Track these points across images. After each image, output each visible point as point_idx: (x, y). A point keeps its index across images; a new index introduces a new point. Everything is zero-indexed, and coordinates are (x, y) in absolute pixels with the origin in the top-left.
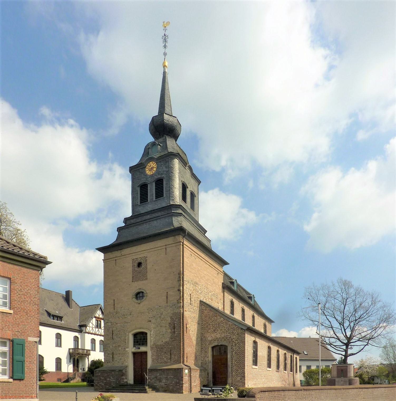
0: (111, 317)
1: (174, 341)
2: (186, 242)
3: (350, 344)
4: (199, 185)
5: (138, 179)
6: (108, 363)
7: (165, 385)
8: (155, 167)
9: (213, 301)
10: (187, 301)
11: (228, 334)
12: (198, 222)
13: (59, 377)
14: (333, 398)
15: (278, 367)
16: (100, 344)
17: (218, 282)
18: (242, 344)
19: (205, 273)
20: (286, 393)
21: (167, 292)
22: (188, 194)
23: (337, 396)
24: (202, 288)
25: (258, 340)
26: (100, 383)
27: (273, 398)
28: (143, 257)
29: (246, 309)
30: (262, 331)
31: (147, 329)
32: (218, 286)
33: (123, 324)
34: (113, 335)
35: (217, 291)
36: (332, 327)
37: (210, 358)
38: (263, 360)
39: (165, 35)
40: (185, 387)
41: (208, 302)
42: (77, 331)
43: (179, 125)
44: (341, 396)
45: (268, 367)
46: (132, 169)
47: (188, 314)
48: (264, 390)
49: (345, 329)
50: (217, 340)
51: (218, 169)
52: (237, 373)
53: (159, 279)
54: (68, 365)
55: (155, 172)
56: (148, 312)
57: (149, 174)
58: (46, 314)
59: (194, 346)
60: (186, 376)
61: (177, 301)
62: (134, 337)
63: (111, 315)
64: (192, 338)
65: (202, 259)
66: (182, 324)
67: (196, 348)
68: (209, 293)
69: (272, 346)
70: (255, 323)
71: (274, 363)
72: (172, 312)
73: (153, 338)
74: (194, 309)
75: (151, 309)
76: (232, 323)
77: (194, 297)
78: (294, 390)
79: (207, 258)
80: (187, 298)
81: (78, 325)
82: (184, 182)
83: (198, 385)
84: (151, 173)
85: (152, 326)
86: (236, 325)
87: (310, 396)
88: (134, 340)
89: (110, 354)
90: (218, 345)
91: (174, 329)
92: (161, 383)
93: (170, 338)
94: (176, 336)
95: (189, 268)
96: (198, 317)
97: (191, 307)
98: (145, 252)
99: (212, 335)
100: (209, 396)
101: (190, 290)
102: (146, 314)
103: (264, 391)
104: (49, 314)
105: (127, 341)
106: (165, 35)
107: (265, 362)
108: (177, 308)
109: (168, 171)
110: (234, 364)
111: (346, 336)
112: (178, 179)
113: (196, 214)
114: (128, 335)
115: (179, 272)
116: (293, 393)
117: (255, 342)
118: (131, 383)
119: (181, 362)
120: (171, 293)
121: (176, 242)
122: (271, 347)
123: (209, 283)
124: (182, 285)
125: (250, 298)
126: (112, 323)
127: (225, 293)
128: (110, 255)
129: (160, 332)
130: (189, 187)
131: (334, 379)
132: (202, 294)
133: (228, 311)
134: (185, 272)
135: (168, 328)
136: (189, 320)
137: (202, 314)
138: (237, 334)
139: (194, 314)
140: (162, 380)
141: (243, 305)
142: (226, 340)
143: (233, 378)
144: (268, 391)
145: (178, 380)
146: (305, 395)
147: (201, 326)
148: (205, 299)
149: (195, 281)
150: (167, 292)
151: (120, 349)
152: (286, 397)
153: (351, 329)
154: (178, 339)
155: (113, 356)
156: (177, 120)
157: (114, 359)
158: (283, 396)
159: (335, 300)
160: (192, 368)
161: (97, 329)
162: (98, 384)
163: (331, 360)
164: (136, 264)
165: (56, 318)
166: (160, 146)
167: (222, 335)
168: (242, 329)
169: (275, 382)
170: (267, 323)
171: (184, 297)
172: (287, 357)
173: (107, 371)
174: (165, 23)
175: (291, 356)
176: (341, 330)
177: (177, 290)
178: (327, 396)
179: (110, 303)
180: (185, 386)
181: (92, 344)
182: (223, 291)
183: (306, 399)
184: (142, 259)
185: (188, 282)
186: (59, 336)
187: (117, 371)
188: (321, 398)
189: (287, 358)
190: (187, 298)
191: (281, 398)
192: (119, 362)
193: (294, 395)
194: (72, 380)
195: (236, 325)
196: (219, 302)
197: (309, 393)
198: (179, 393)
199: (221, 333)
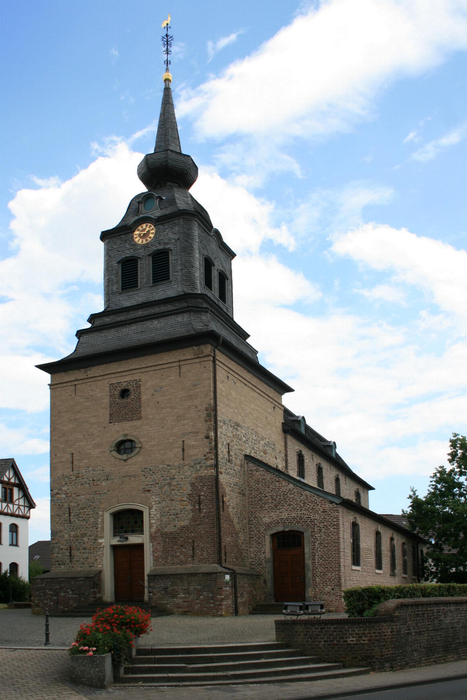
5: (118, 251)
6: (59, 564)
7: (184, 602)
9: (267, 454)
11: (305, 512)
12: (232, 319)
16: (10, 531)
18: (333, 528)
19: (253, 406)
21: (183, 441)
22: (215, 275)
24: (248, 433)
26: (46, 601)
28: (132, 381)
32: (274, 429)
34: (70, 515)
38: (369, 555)
40: (225, 605)
41: (258, 457)
47: (226, 479)
52: (324, 578)
53: (167, 419)
55: (152, 240)
57: (140, 242)
60: (227, 586)
61: (205, 456)
64: (234, 519)
65: (247, 383)
68: (260, 441)
71: (386, 561)
73: (154, 519)
74: (235, 470)
75: (150, 470)
77: (235, 449)
82: (208, 256)
84: (144, 241)
85: (153, 499)
89: (65, 549)
90: (285, 530)
91: (200, 503)
92: (175, 600)
93: (191, 519)
95: (225, 399)
98: (136, 371)
99: (272, 514)
101: (228, 437)
102: (140, 478)
105: (99, 526)
107: (372, 559)
108: (204, 467)
113: (229, 307)
114: (103, 516)
117: (355, 526)
120: (191, 442)
122: (381, 533)
123: (260, 425)
126: (68, 495)
129: (169, 510)
130: (216, 264)
132: (248, 444)
133: (293, 473)
134: (219, 405)
135: (186, 503)
136: (228, 490)
137: (250, 477)
138: (321, 512)
139: (236, 478)
140: (177, 593)
142: (300, 522)
143: (317, 589)
145: (212, 593)
148: (253, 451)
149: (235, 420)
150: (183, 441)
151: (87, 540)
154: (208, 522)
155: (70, 553)
157: (73, 558)
161: (4, 505)
162: (41, 603)
164: (117, 393)
173: (61, 579)
177: (203, 437)
179: (64, 459)
180: (226, 603)
184: (131, 384)
185: (224, 424)
196: (277, 457)
199: (290, 510)
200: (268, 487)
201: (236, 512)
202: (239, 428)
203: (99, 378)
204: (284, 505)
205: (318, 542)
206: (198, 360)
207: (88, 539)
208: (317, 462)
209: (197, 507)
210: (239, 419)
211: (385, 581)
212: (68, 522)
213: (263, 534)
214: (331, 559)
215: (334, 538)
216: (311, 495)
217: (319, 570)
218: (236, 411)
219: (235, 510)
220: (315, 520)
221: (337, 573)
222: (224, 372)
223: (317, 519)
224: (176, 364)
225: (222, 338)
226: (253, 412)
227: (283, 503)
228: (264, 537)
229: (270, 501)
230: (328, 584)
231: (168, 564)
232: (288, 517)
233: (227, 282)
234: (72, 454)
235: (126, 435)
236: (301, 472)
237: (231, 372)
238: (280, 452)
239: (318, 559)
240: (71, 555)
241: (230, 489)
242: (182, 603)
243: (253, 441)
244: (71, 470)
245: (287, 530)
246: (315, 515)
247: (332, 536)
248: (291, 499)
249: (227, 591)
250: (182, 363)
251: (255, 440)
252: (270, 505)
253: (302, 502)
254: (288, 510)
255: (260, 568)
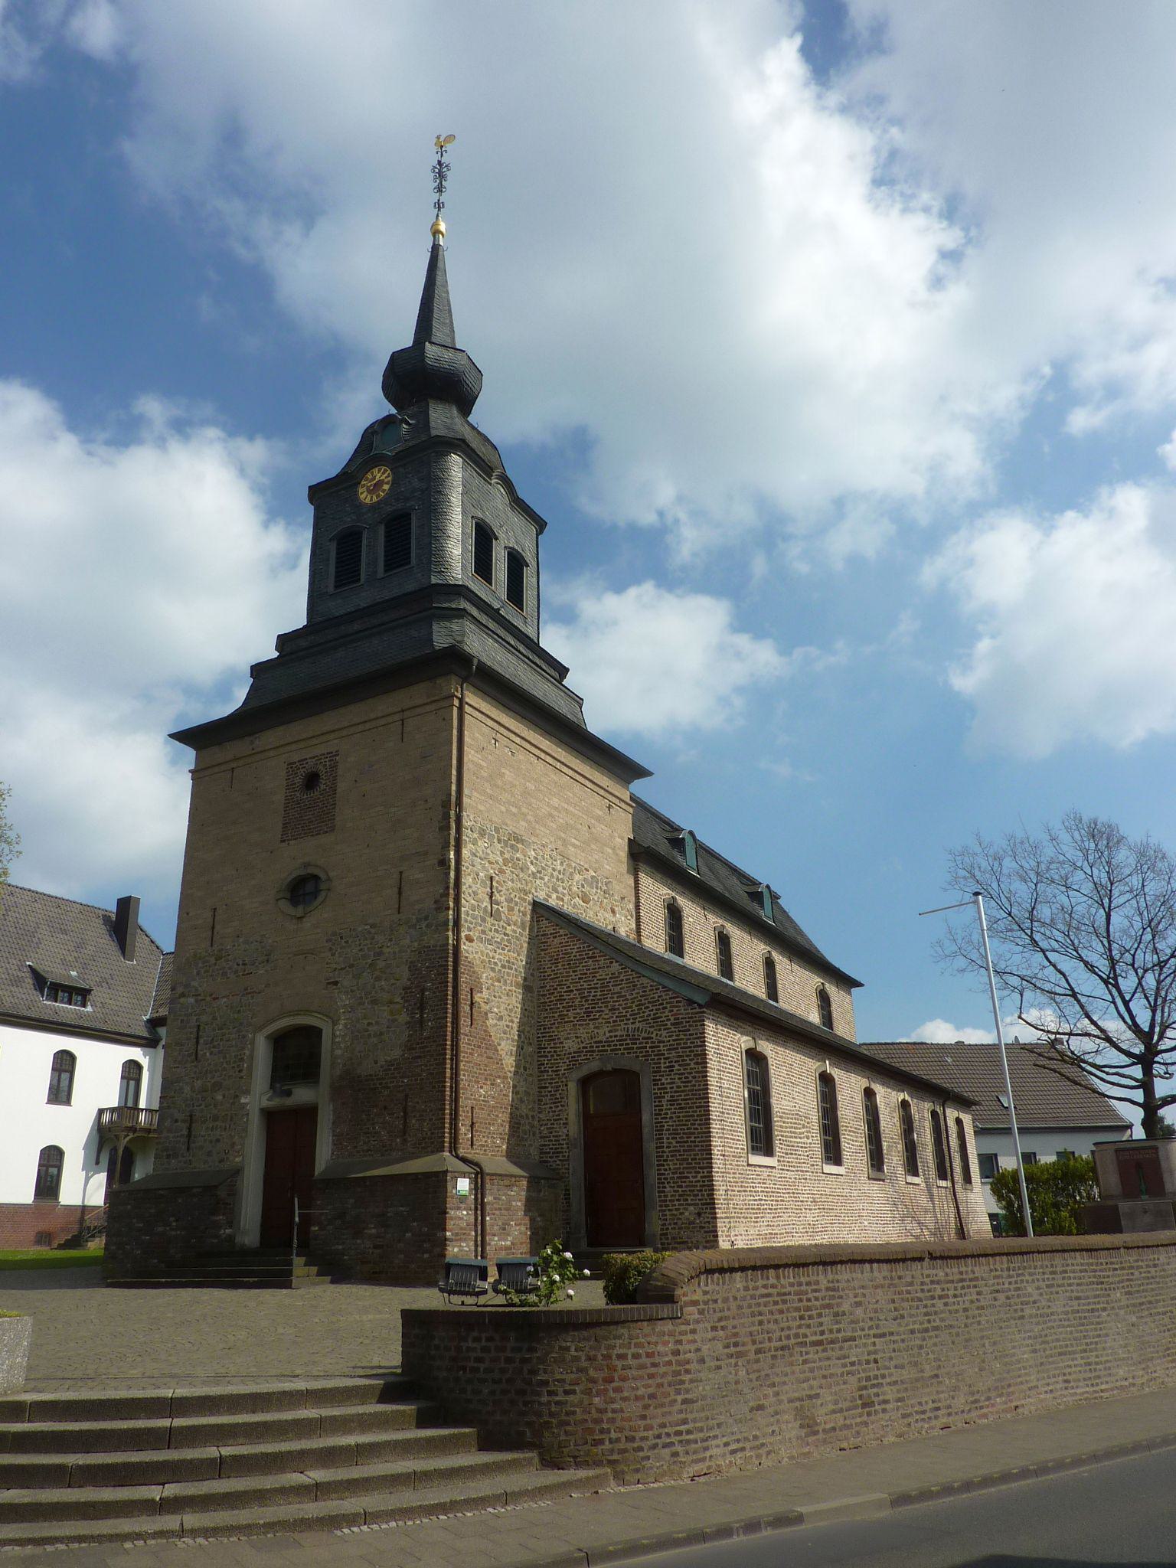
0: (198, 974)
1: (420, 1057)
2: (471, 698)
3: (1156, 1059)
4: (540, 532)
7: (376, 1247)
8: (386, 480)
10: (476, 903)
13: (43, 1225)
14: (1082, 1291)
15: (876, 1159)
17: (612, 836)
19: (555, 802)
20: (839, 1277)
21: (401, 873)
23: (1102, 1283)
24: (543, 857)
25: (766, 1047)
27: (776, 1303)
29: (736, 933)
30: (814, 1017)
31: (319, 1013)
32: (610, 851)
33: (239, 997)
35: (608, 867)
36: (1074, 995)
37: (573, 1126)
38: (803, 1130)
39: (439, 163)
41: (567, 909)
42: (139, 1041)
43: (474, 373)
44: (1122, 1281)
45: (753, 1148)
46: (319, 493)
48: (720, 1265)
49: (1127, 998)
50: (599, 1051)
51: (649, 518)
52: (681, 1187)
54: (87, 1174)
56: (331, 949)
57: (367, 501)
58: (31, 981)
59: (506, 1078)
61: (435, 902)
62: (275, 1051)
63: (200, 965)
64: (500, 1045)
65: (542, 755)
66: (450, 988)
67: (514, 1086)
68: (571, 874)
69: (836, 1073)
70: (779, 986)
71: (853, 1143)
72: (416, 944)
73: (341, 1048)
74: (505, 934)
76: (653, 981)
78: (878, 1261)
79: (560, 753)
80: (474, 892)
81: (148, 1017)
83: (521, 1243)
84: (374, 497)
85: (342, 1001)
86: (670, 990)
87: (969, 1287)
88: (275, 1059)
91: (422, 1008)
94: (429, 1038)
96: (527, 963)
97: (493, 925)
98: (332, 736)
100: (482, 1300)
101: (490, 863)
102: (322, 955)
103: (722, 1271)
104: (40, 981)
106: (439, 163)
107: (814, 1140)
109: (427, 489)
110: (667, 1150)
111: (1135, 1028)
112: (459, 510)
114: (253, 1043)
115: (444, 798)
116: (876, 1274)
117: (755, 1058)
118: (246, 1242)
119: (444, 1147)
121: (437, 698)
122: (835, 1077)
123: (573, 840)
124: (452, 842)
125: (757, 897)
126: (200, 998)
127: (641, 875)
128: (218, 754)
130: (501, 534)
131: (1110, 1203)
133: (655, 942)
135: (398, 1006)
137: (542, 950)
138: (671, 1024)
141: (721, 922)
143: (668, 1213)
144: (743, 1269)
146: (938, 1282)
147: (539, 999)
148: (554, 896)
149: (510, 829)
150: (401, 873)
152: (841, 1297)
153: (1147, 998)
156: (466, 357)
158: (828, 1289)
159: (1071, 893)
160: (487, 1170)
162: (121, 1252)
163: (1111, 1127)
164: (298, 781)
165: (80, 998)
166: (407, 423)
167: (617, 1030)
168: (691, 1002)
169: (866, 1223)
170: (832, 990)
171: (464, 888)
172: (916, 1117)
174: (442, 139)
175: (934, 1114)
176: (1114, 1002)
177: (436, 861)
178: (1052, 1286)
181: (60, 1076)
182: (632, 869)
183: (946, 1304)
186: (64, 1063)
187: (195, 1190)
188: (1025, 1295)
189: (916, 1124)
190: (474, 892)
191: (817, 1299)
192: (209, 1154)
193: (882, 1286)
194: (93, 1236)
195: (670, 990)
196: (616, 909)
197: (961, 1273)
198: (286, 1288)
199: (614, 1021)
200: (574, 972)
201: (508, 1026)
202: (520, 846)
203: (272, 753)
204: (602, 1011)
205: (667, 1097)
206: (433, 707)
207: (224, 1097)
208: (716, 923)
209: (418, 1016)
210: (521, 828)
211: (855, 1193)
212: (194, 1057)
213: (564, 1080)
214: (693, 1139)
215: (697, 1088)
216: (651, 986)
217: (672, 1167)
218: (514, 810)
219: (503, 1023)
220: (661, 1045)
221: (705, 1174)
222: (486, 730)
223: (664, 1042)
224: (397, 717)
225: (475, 662)
226: (556, 813)
227: (600, 1005)
228: (566, 1085)
229: (577, 1003)
230: (689, 1202)
231: (358, 1152)
232: (611, 1037)
233: (527, 570)
234: (215, 909)
235: (306, 865)
236: (676, 943)
237: (502, 730)
238: (623, 898)
239: (668, 1139)
240: (189, 1135)
241: (492, 974)
242: (371, 1251)
243: (555, 874)
244: (209, 943)
245: (609, 1067)
246: (659, 1033)
247: (693, 1083)
248: (615, 996)
249: (461, 1219)
250: (407, 714)
251: (560, 872)
252: (578, 1011)
253: (636, 1003)
254: (609, 1022)
255: (558, 1162)
